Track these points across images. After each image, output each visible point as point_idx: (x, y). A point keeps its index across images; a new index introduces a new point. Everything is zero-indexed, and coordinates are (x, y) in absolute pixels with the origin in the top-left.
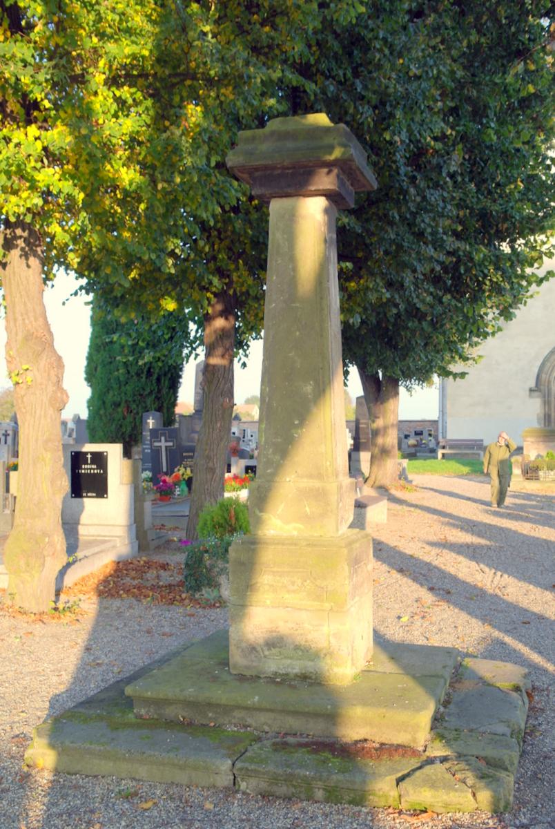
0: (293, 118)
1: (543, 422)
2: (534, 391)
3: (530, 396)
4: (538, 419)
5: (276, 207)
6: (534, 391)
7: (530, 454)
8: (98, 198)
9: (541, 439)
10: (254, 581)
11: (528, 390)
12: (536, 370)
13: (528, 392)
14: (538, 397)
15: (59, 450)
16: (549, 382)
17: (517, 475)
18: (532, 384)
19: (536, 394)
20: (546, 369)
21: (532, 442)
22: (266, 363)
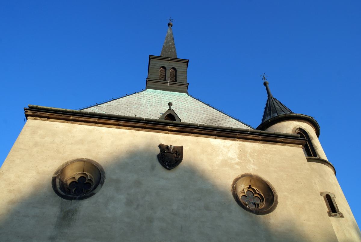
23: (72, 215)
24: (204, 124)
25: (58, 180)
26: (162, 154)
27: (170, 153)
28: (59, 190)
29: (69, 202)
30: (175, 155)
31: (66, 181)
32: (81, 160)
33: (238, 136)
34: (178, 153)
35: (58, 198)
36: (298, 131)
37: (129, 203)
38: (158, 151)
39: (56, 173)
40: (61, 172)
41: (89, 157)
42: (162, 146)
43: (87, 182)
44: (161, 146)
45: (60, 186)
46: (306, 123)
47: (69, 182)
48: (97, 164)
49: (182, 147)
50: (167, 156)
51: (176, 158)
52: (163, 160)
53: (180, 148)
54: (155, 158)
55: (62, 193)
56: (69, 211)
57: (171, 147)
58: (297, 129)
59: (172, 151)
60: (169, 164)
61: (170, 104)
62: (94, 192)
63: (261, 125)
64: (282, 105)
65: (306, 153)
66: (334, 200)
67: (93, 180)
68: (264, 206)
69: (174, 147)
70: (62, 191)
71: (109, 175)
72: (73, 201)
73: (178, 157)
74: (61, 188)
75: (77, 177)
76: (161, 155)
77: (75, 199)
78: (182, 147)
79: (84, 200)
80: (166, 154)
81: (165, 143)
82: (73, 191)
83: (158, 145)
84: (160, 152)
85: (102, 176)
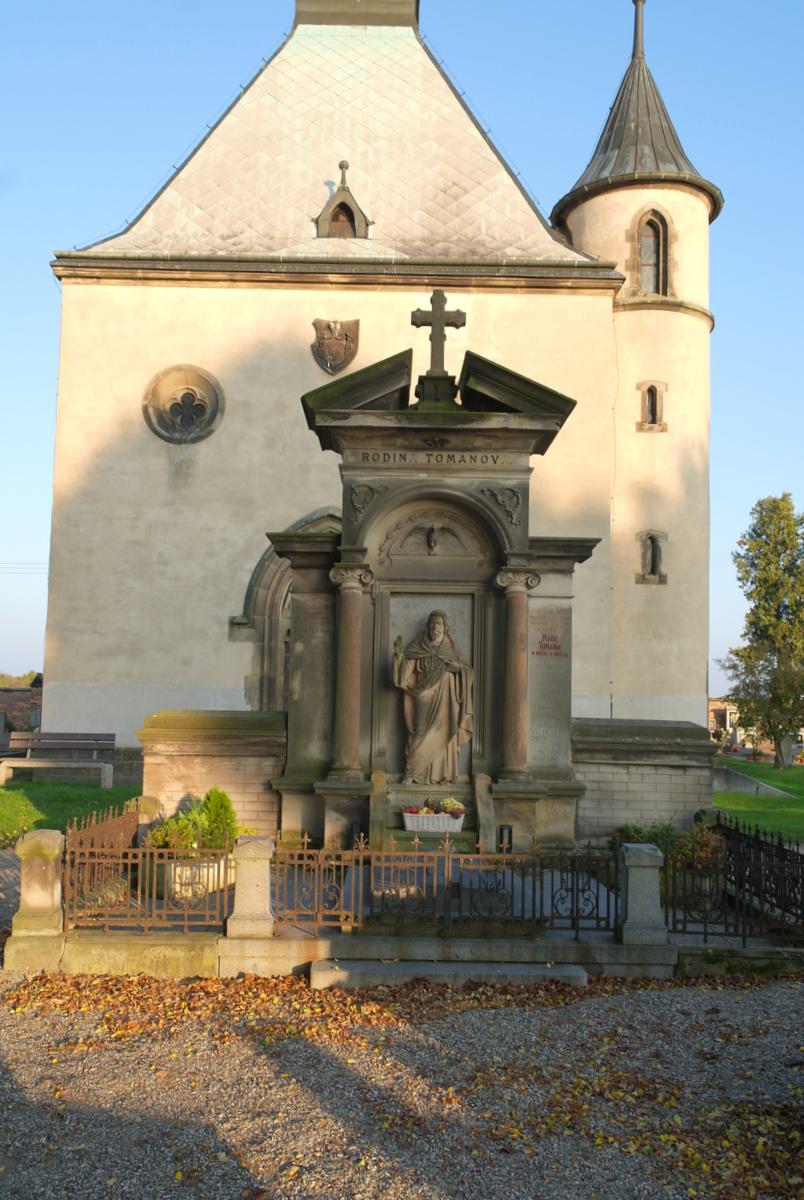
0: (570, 748)
1: (256, 696)
2: (238, 624)
3: (232, 637)
4: (248, 690)
5: (574, 721)
6: (238, 624)
7: (162, 799)
8: (525, 858)
9: (198, 748)
10: (519, 725)
11: (227, 620)
12: (246, 579)
13: (226, 628)
14: (248, 638)
15: (148, 773)
16: (273, 605)
17: (37, 914)
18: (236, 608)
19: (245, 632)
20: (266, 579)
21: (170, 757)
22: (388, 366)
23: (188, 468)
24: (174, 942)
25: (151, 410)
28: (158, 428)
29: (179, 447)
30: (344, 342)
31: (164, 406)
32: (178, 369)
33: (474, 283)
35: (161, 442)
36: (650, 217)
37: (270, 443)
38: (311, 336)
39: (146, 398)
40: (153, 393)
41: (195, 363)
43: (196, 402)
44: (316, 325)
45: (158, 419)
46: (676, 189)
47: (168, 406)
48: (209, 375)
49: (357, 323)
54: (308, 351)
55: (163, 432)
56: (182, 462)
58: (647, 213)
61: (343, 166)
62: (213, 427)
63: (567, 195)
64: (658, 95)
66: (662, 398)
67: (207, 401)
69: (342, 324)
70: (163, 428)
71: (231, 397)
72: (183, 446)
74: (160, 424)
75: (179, 397)
77: (185, 442)
78: (357, 323)
81: (325, 316)
82: (179, 420)
85: (219, 397)
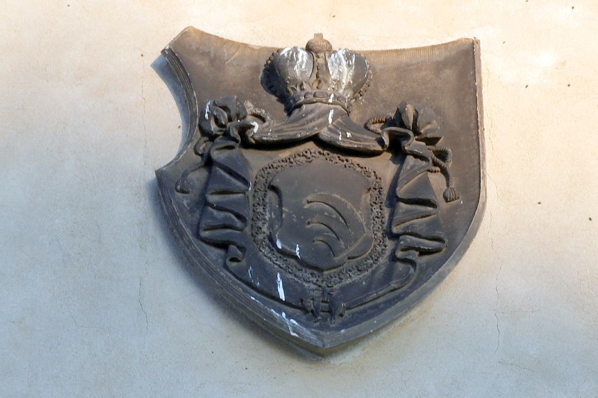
26: (209, 163)
27: (316, 139)
34: (413, 144)
42: (202, 63)
50: (274, 189)
51: (393, 199)
52: (223, 245)
53: (439, 66)
57: (320, 72)
59: (345, 125)
60: (310, 284)
65: (362, 157)
68: (338, 194)
69: (359, 61)
73: (425, 184)
76: (198, 177)
79: (283, 151)
80: (257, 161)
83: (155, 54)
84: (188, 139)
